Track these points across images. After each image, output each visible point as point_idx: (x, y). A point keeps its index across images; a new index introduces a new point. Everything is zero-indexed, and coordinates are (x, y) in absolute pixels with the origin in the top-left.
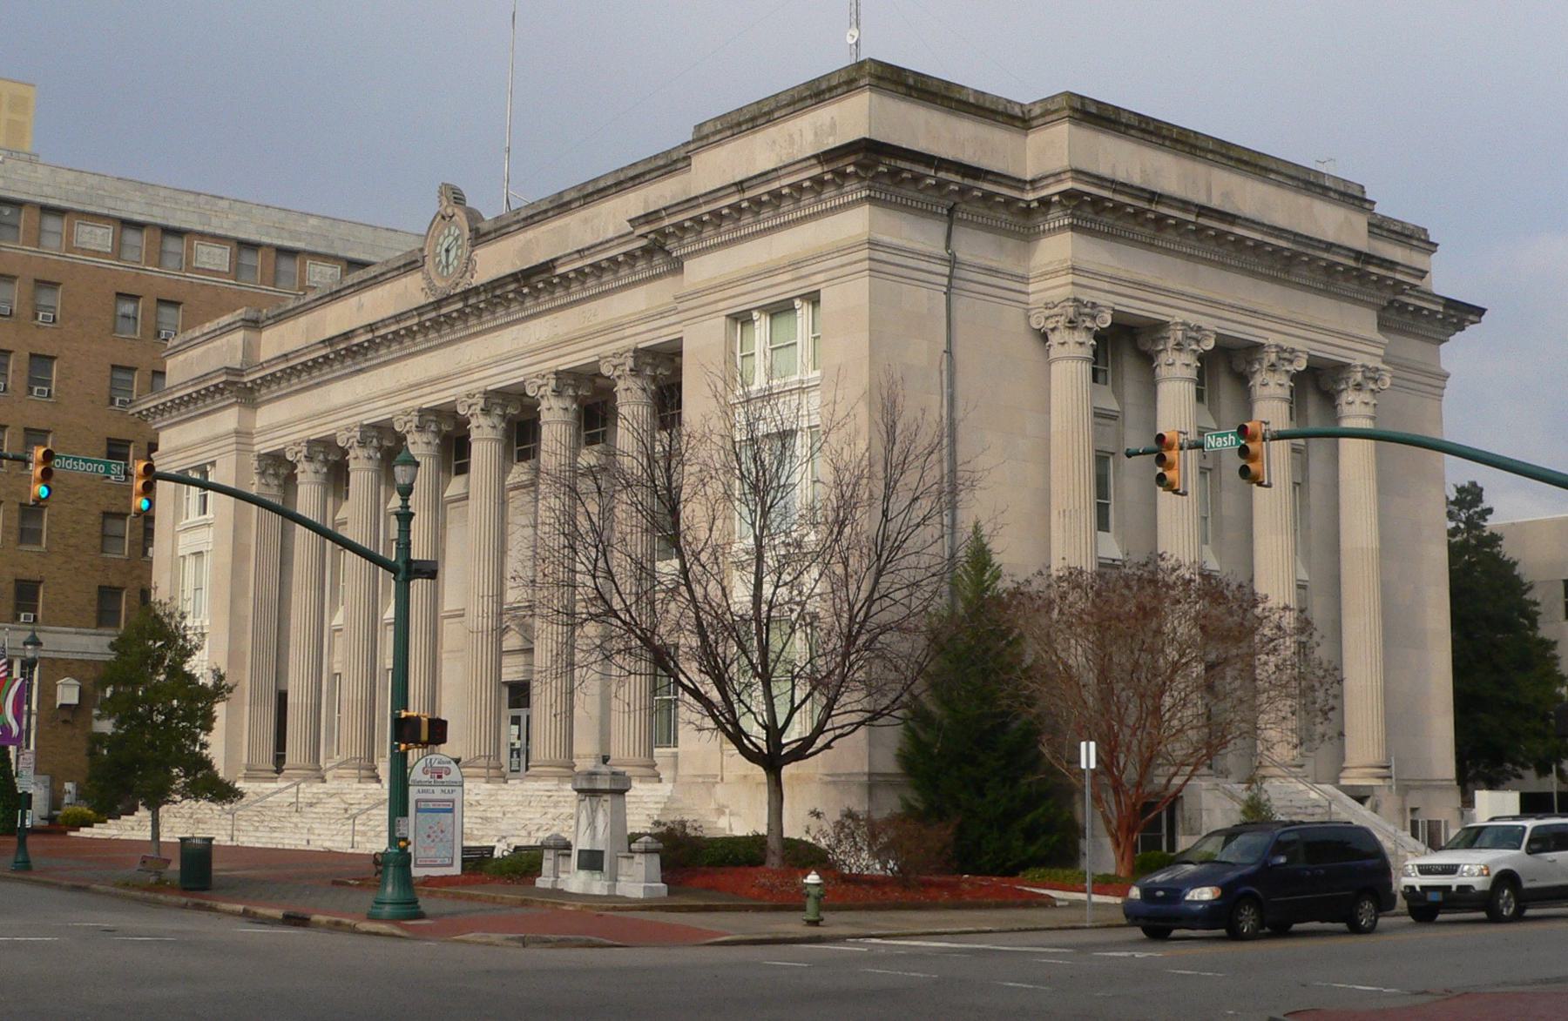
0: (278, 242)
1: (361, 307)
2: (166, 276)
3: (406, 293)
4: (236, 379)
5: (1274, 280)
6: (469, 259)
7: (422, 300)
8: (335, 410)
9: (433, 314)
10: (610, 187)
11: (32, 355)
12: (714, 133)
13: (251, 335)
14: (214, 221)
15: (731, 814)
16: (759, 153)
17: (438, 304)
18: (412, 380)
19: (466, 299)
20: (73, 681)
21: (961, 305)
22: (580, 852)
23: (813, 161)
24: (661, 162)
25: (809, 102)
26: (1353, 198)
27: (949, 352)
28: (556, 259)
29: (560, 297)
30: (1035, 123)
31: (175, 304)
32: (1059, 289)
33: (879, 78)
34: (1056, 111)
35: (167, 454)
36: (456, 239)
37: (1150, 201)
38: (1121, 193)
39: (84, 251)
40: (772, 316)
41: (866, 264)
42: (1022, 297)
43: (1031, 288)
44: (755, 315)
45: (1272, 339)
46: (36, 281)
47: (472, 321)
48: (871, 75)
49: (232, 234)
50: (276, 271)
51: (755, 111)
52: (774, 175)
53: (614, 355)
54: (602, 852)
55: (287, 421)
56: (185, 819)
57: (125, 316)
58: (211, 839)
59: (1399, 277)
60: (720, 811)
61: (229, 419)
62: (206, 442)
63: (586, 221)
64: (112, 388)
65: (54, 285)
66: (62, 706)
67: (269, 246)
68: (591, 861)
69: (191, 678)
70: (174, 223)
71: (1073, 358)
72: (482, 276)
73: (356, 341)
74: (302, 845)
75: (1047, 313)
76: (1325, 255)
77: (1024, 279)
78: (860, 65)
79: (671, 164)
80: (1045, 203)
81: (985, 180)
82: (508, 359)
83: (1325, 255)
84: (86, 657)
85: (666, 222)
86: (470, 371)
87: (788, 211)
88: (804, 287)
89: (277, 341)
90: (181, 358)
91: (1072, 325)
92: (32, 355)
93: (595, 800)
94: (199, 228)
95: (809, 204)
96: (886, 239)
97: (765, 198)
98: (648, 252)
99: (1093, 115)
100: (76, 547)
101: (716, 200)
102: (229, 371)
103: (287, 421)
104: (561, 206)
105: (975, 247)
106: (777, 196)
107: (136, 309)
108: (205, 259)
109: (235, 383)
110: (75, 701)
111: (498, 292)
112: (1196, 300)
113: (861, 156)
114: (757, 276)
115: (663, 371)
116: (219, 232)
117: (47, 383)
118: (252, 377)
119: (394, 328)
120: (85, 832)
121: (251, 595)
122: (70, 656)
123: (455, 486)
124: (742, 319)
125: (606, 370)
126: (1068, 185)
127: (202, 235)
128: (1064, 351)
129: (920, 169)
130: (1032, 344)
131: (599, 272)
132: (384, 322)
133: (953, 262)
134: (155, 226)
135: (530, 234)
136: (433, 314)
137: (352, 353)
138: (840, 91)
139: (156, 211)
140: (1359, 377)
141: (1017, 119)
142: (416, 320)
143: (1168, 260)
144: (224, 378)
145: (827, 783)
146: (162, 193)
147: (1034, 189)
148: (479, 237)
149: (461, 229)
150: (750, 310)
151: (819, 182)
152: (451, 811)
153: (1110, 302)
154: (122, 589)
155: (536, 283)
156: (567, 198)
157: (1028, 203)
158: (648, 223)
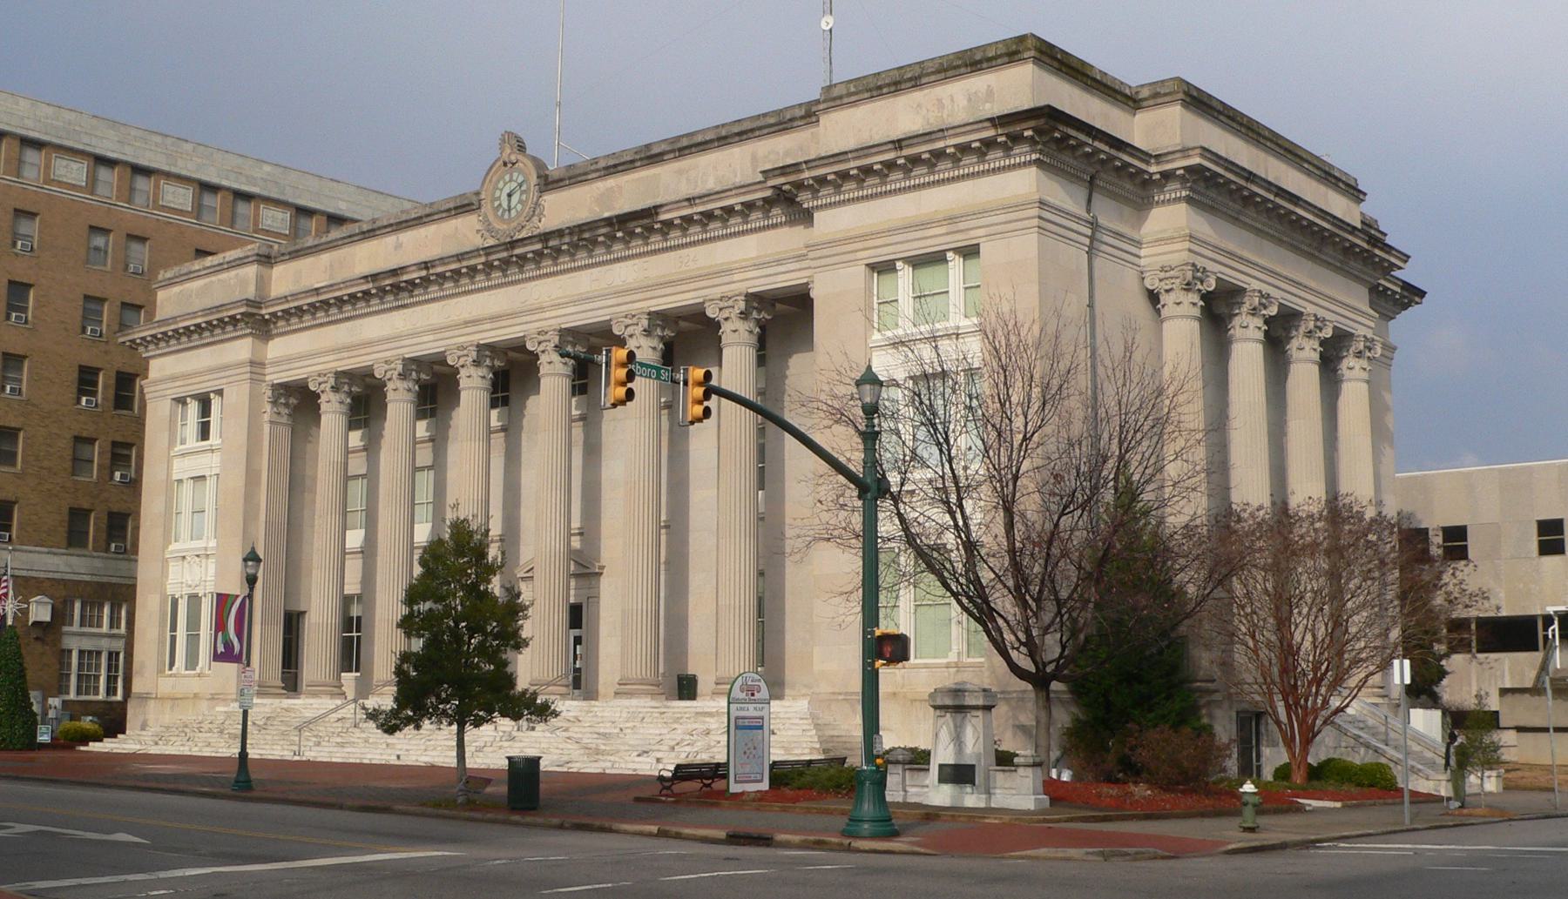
0: (235, 186)
1: (398, 246)
3: (464, 233)
5: (1310, 256)
6: (537, 204)
7: (478, 242)
8: (370, 343)
9: (505, 254)
10: (711, 141)
11: (10, 282)
12: (850, 94)
14: (180, 163)
16: (905, 115)
19: (547, 240)
20: (46, 600)
21: (1098, 262)
22: (941, 766)
23: (987, 124)
24: (772, 121)
25: (963, 70)
26: (1354, 192)
27: (1091, 306)
28: (661, 206)
29: (656, 241)
30: (1145, 104)
31: (142, 240)
32: (1177, 254)
33: (1041, 52)
34: (1166, 95)
35: (155, 382)
36: (520, 185)
37: (1247, 180)
38: (1231, 171)
39: (60, 184)
41: (1036, 222)
42: (1135, 260)
43: (1143, 253)
45: (1310, 309)
46: (16, 210)
47: (547, 262)
48: (1036, 49)
49: (194, 176)
50: (234, 214)
51: (896, 76)
54: (973, 767)
55: (306, 353)
56: (494, 745)
57: (97, 249)
58: (535, 762)
59: (1393, 260)
61: (241, 349)
63: (680, 172)
64: (84, 318)
65: (32, 215)
66: (36, 623)
67: (228, 189)
68: (959, 774)
69: (486, 594)
71: (1187, 317)
72: (549, 223)
73: (405, 278)
74: (393, 761)
75: (1162, 275)
76: (1350, 238)
77: (1138, 244)
78: (1021, 39)
80: (1167, 176)
81: (1125, 152)
82: (588, 299)
83: (1350, 238)
84: (57, 576)
85: (806, 174)
86: (542, 309)
87: (945, 169)
88: (961, 240)
89: (287, 279)
90: (176, 289)
91: (1188, 287)
92: (10, 282)
93: (959, 716)
94: (166, 168)
95: (970, 164)
96: (1050, 200)
97: (925, 156)
98: (768, 203)
99: (1199, 102)
100: (49, 469)
101: (866, 156)
102: (249, 302)
103: (306, 353)
104: (650, 157)
105: (1108, 214)
106: (939, 155)
107: (107, 244)
109: (253, 315)
110: (48, 618)
111: (586, 235)
112: (1270, 274)
113: (1042, 121)
115: (784, 318)
116: (184, 173)
117: (24, 310)
118: (271, 310)
119: (454, 266)
120: (94, 747)
121: (262, 517)
122: (42, 575)
124: (884, 268)
125: (711, 312)
126: (1196, 160)
128: (1179, 310)
129: (1082, 137)
130: (1141, 306)
131: (710, 218)
132: (442, 260)
133: (1094, 225)
134: (125, 163)
135: (611, 182)
136: (505, 254)
137: (397, 289)
138: (999, 61)
139: (128, 150)
140: (1361, 346)
141: (1130, 100)
142: (483, 259)
143: (1245, 234)
144: (242, 310)
146: (133, 132)
147: (1158, 163)
148: (548, 183)
149: (525, 175)
151: (989, 144)
152: (761, 728)
153: (1218, 271)
154: (90, 511)
155: (635, 227)
156: (656, 150)
157: (1151, 175)
158: (783, 174)
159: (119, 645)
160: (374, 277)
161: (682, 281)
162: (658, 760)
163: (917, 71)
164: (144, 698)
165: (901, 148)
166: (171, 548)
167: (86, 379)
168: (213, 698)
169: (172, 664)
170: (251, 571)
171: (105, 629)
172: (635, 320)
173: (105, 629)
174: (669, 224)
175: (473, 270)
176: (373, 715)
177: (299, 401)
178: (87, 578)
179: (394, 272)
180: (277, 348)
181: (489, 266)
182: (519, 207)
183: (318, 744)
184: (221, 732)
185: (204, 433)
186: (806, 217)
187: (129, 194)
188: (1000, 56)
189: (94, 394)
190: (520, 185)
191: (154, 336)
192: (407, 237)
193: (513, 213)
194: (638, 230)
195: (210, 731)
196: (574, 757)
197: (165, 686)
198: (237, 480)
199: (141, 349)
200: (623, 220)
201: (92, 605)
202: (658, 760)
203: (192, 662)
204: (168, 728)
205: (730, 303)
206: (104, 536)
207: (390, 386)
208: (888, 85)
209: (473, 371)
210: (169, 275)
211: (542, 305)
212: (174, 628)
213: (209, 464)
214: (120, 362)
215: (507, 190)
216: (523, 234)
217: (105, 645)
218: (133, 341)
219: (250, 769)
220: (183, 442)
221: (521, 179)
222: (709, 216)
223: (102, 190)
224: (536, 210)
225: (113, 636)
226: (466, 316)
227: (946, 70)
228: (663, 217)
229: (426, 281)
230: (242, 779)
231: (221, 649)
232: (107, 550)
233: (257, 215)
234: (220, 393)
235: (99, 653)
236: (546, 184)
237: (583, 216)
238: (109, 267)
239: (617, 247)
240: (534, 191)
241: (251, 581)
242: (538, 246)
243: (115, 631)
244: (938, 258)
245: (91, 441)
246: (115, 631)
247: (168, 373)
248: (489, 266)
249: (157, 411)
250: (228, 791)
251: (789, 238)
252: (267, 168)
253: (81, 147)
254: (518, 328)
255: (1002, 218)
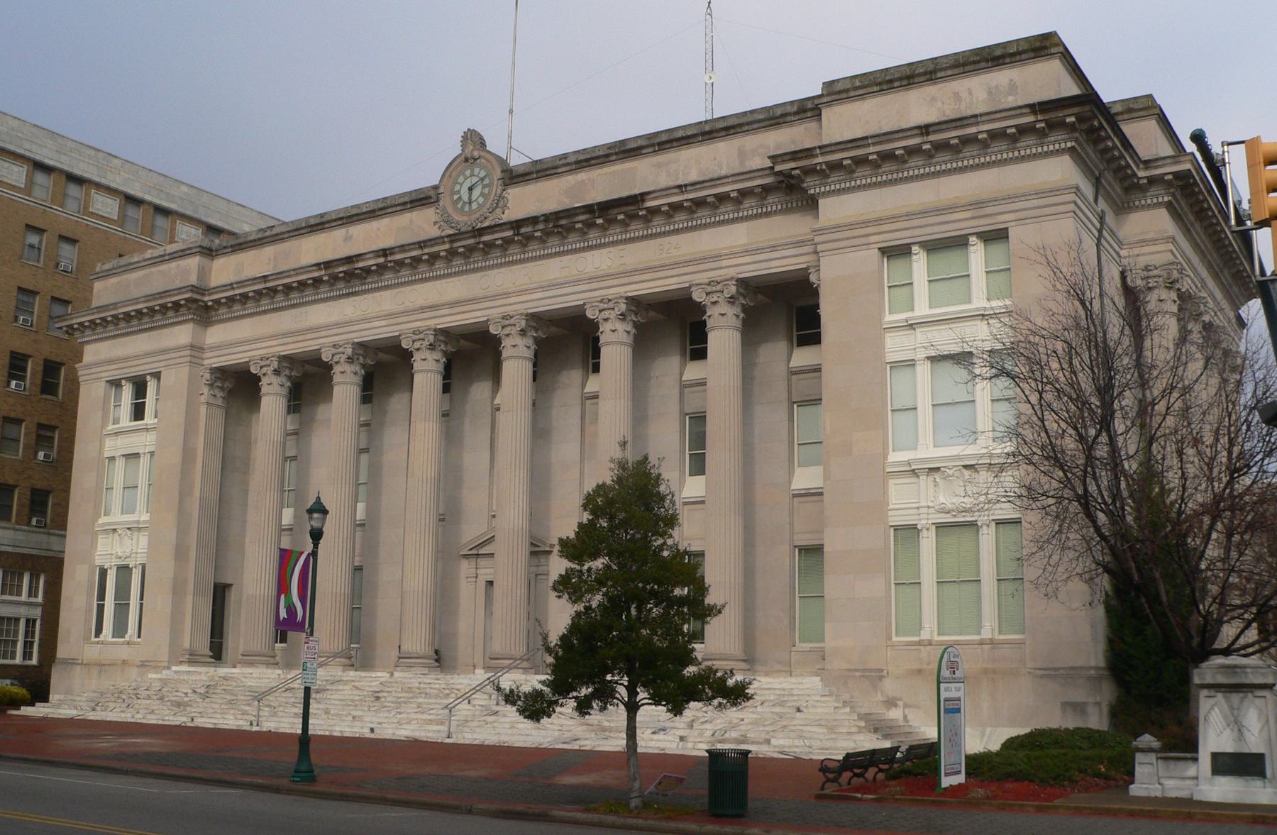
0: (157, 201)
1: (347, 239)
2: (68, 212)
3: (422, 224)
4: (198, 297)
6: (501, 197)
7: (435, 232)
8: (318, 328)
9: (472, 241)
13: (205, 261)
15: (906, 706)
17: (453, 238)
18: (431, 301)
22: (1215, 756)
23: (1027, 110)
24: (761, 117)
25: (983, 65)
28: (649, 193)
29: (636, 228)
31: (72, 241)
34: (1141, 110)
35: (90, 366)
36: (482, 179)
40: (928, 251)
44: (123, 382)
49: (121, 188)
52: (973, 120)
53: (709, 284)
57: (31, 246)
60: (891, 703)
61: (182, 334)
62: (147, 355)
63: (659, 165)
67: (150, 203)
70: (77, 172)
73: (361, 265)
79: (807, 110)
80: (1152, 181)
85: (820, 159)
87: (970, 155)
90: (113, 280)
94: (97, 179)
95: (999, 150)
102: (194, 289)
103: (250, 339)
107: (40, 242)
108: (99, 206)
109: (196, 301)
111: (563, 222)
114: (909, 216)
116: (113, 185)
120: (26, 711)
121: (197, 493)
123: (593, 385)
124: (116, 384)
125: (698, 296)
127: (98, 186)
132: (403, 248)
134: (61, 171)
135: (582, 176)
136: (472, 241)
137: (350, 276)
138: (1024, 56)
139: (63, 158)
142: (447, 246)
145: (1042, 677)
146: (69, 144)
147: (1147, 168)
150: (909, 244)
151: (1023, 130)
158: (794, 159)
159: (37, 612)
160: (327, 265)
161: (663, 267)
162: (682, 739)
163: (931, 67)
164: (70, 663)
165: (928, 134)
166: (100, 521)
167: (17, 364)
168: (143, 665)
169: (99, 631)
170: (316, 524)
171: (24, 597)
172: (611, 305)
173: (24, 597)
174: (655, 211)
175: (434, 257)
176: (510, 698)
177: (239, 386)
178: (10, 549)
179: (349, 260)
180: (216, 334)
181: (452, 253)
182: (481, 200)
183: (275, 715)
184: (161, 699)
185: (138, 412)
186: (811, 204)
187: (61, 199)
188: (1025, 52)
189: (22, 378)
190: (482, 179)
191: (92, 322)
192: (357, 230)
193: (474, 206)
194: (621, 217)
195: (149, 697)
196: (580, 735)
197: (91, 652)
198: (173, 456)
199: (77, 334)
200: (605, 208)
201: (13, 573)
202: (682, 739)
203: (120, 629)
204: (102, 693)
205: (719, 287)
206: (27, 510)
207: (337, 369)
208: (900, 79)
209: (427, 354)
210: (107, 267)
211: (510, 292)
212: (102, 596)
213: (144, 442)
214: (48, 351)
215: (468, 184)
216: (486, 224)
217: (23, 612)
218: (70, 327)
219: (314, 758)
220: (116, 421)
221: (483, 174)
222: (700, 203)
223: (38, 193)
224: (500, 202)
225: (30, 604)
226: (421, 302)
227: (964, 65)
228: (650, 204)
229: (382, 268)
230: (304, 767)
231: (283, 614)
232: (29, 524)
233: (173, 230)
234: (157, 376)
235: (17, 620)
236: (512, 178)
237: (551, 206)
238: (41, 265)
239: (593, 234)
240: (497, 188)
241: (317, 535)
242: (510, 233)
243: (32, 600)
244: (959, 242)
245: (18, 422)
246: (32, 600)
247: (101, 358)
248: (452, 253)
249: (91, 393)
250: (285, 782)
251: (790, 226)
252: (184, 189)
253: (22, 152)
254: (479, 314)
255: (1035, 203)
